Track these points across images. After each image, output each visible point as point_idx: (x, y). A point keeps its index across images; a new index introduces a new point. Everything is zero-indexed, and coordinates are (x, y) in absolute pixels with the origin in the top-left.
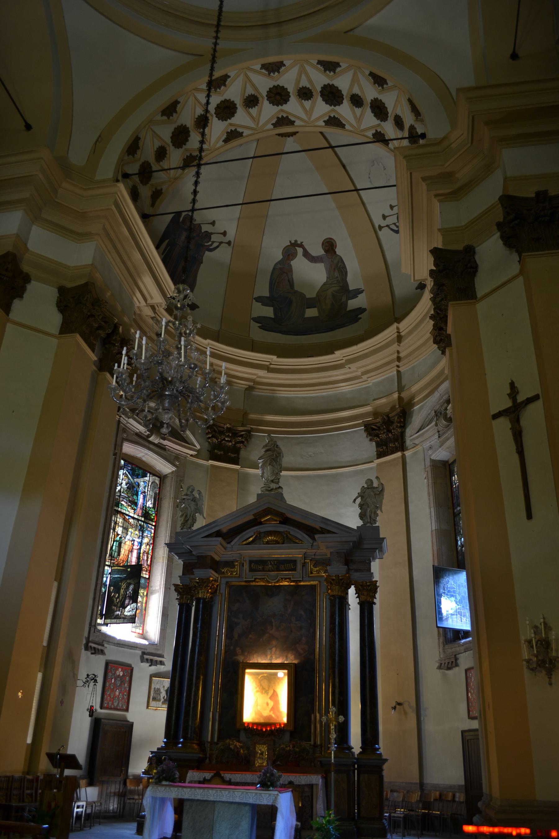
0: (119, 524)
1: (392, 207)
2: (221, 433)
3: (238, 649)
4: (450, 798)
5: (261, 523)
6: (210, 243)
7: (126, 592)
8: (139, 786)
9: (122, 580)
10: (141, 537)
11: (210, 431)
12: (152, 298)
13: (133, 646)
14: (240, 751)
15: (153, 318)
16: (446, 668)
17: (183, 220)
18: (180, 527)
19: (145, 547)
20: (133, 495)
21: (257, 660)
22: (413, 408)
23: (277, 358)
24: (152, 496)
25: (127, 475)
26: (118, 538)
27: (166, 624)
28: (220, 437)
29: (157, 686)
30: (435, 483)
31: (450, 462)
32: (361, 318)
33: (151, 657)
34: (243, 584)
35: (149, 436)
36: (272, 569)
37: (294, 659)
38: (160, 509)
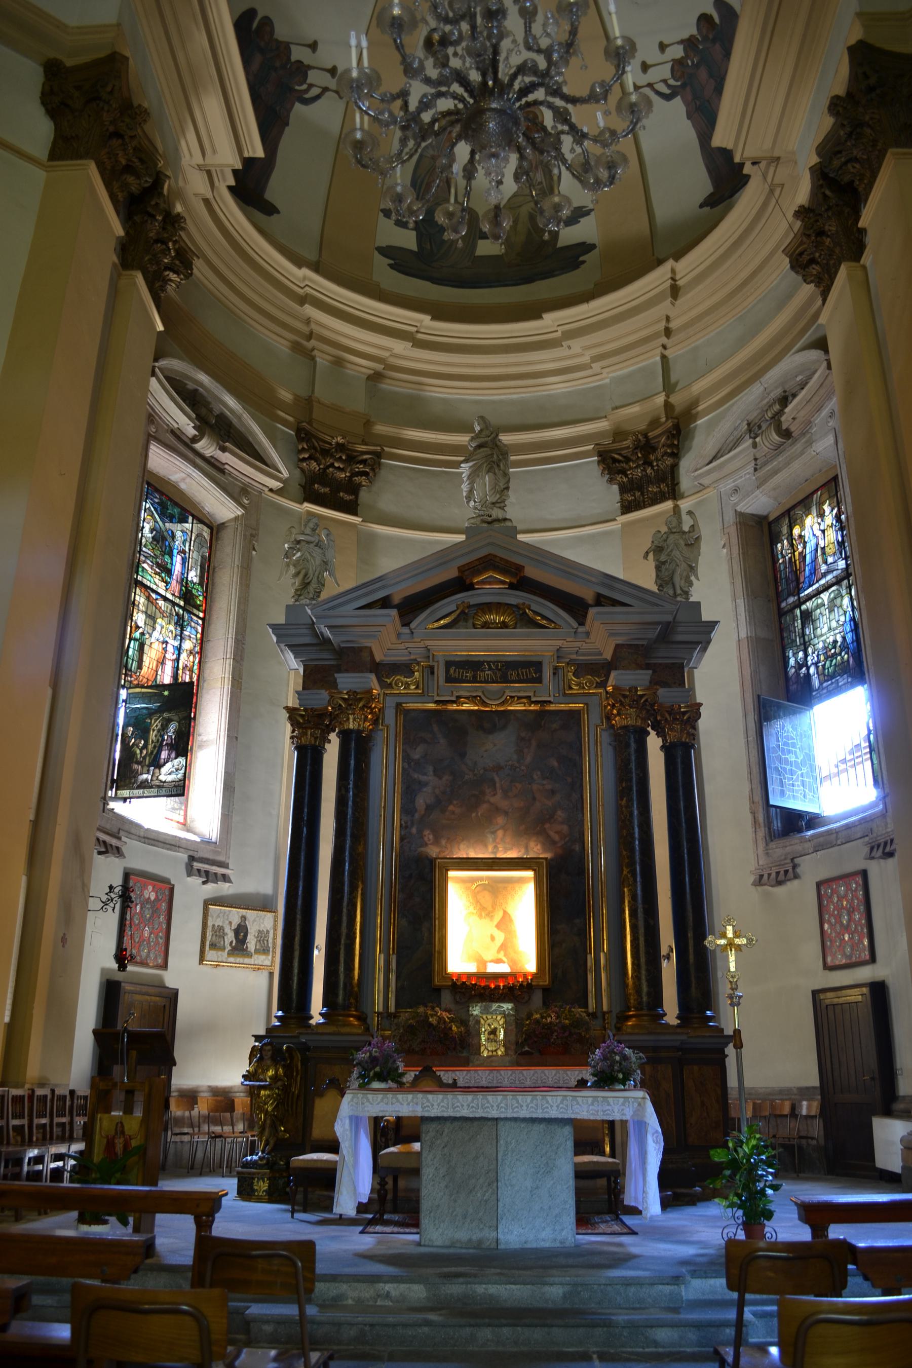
0: (138, 606)
1: (662, 47)
2: (326, 453)
3: (426, 832)
4: (787, 1110)
5: (471, 587)
6: (304, 87)
7: (162, 736)
8: (193, 1109)
9: (151, 713)
10: (179, 638)
11: (305, 446)
12: (214, 151)
13: (173, 843)
14: (451, 1028)
15: (206, 201)
16: (774, 882)
17: (258, 26)
19: (186, 658)
21: (467, 854)
22: (695, 421)
23: (431, 320)
26: (137, 635)
27: (231, 804)
28: (323, 461)
29: (219, 923)
30: (744, 554)
31: (771, 518)
32: (583, 262)
34: (432, 706)
35: (195, 440)
37: (541, 851)
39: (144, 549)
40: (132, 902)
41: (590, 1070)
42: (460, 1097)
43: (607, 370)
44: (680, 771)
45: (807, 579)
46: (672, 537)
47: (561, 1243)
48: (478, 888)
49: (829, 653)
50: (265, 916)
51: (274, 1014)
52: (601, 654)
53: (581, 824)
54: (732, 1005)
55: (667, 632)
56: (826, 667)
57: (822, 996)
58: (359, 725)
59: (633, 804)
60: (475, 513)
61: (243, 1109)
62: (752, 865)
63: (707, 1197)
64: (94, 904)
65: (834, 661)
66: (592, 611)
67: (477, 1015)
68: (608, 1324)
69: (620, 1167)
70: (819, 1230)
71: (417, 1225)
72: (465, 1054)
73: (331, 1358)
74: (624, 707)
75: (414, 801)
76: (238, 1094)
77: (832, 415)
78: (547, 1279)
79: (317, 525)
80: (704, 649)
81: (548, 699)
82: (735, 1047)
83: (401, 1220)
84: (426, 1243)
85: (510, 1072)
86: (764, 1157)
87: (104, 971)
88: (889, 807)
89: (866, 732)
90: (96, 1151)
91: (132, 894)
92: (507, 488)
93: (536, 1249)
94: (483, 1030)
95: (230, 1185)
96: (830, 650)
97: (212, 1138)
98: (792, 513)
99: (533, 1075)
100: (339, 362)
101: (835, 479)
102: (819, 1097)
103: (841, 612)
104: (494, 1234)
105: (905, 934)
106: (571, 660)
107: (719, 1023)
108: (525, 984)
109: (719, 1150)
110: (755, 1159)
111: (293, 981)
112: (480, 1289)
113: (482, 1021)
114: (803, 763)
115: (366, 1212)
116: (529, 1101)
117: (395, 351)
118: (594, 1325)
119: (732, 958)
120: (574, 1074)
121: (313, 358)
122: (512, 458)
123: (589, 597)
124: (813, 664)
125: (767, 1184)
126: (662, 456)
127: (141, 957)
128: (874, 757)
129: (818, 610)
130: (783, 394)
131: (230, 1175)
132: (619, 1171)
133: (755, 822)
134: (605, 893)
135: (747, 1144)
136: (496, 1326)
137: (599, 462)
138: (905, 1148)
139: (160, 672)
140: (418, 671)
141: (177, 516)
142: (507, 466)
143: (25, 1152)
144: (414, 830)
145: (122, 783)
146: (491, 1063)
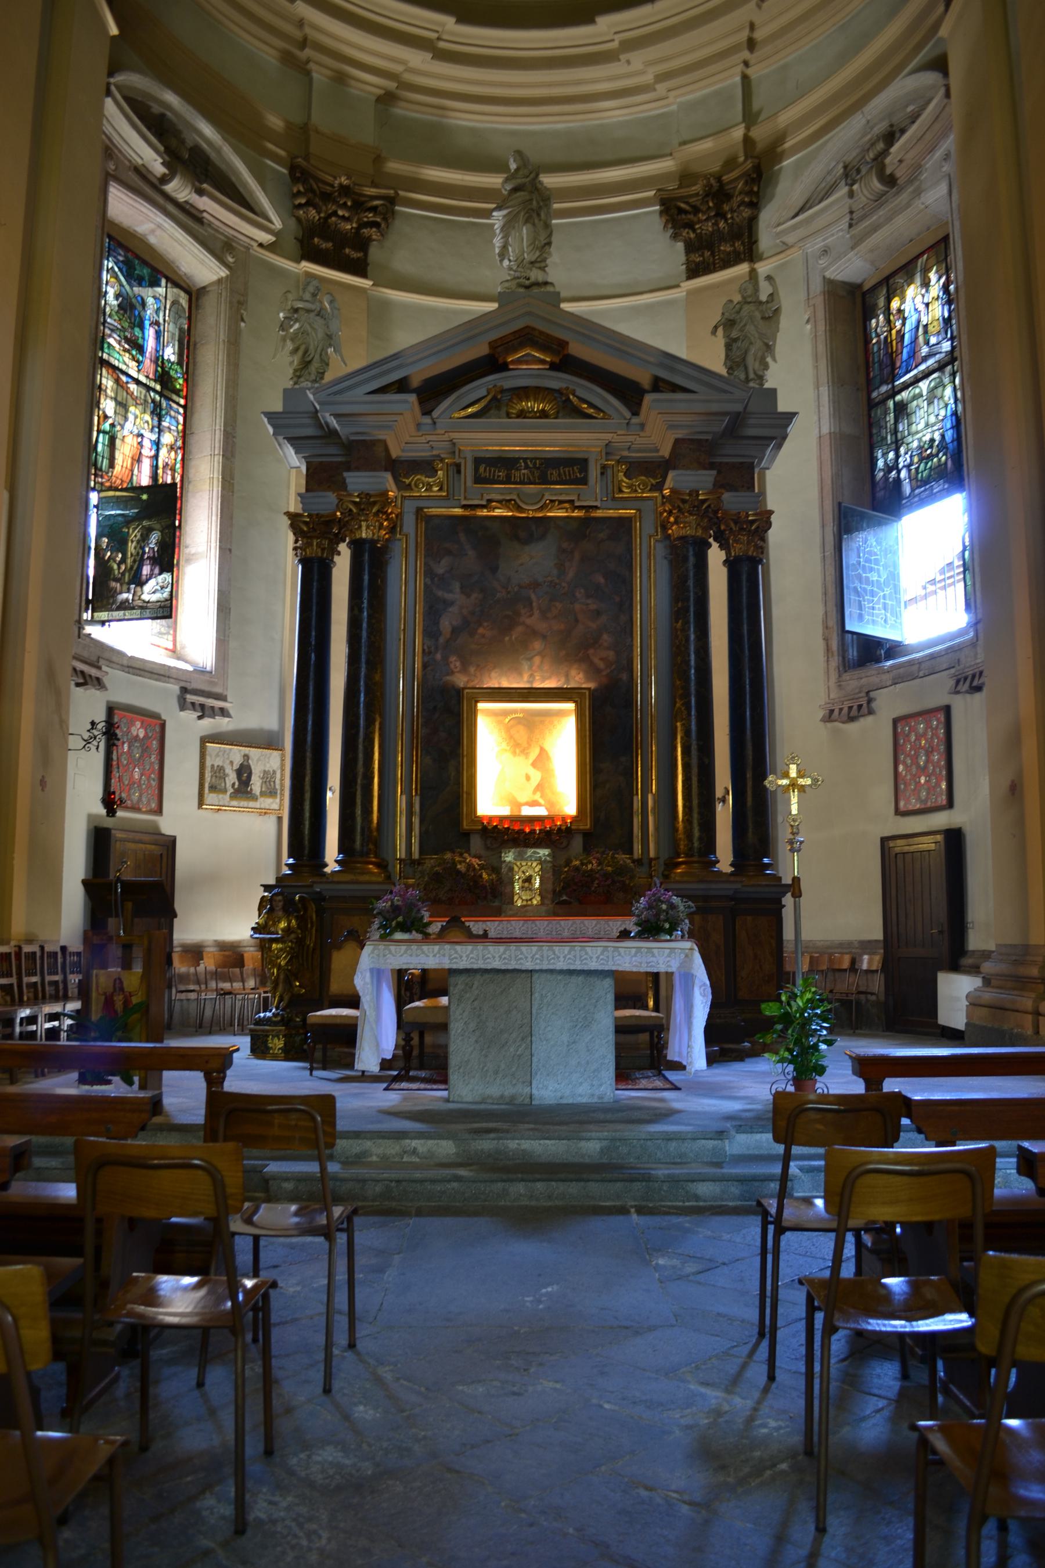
0: (105, 391)
2: (327, 197)
3: (453, 659)
4: (846, 964)
5: (504, 367)
7: (143, 548)
8: (199, 965)
9: (128, 521)
10: (157, 430)
11: (302, 189)
14: (481, 876)
18: (292, 379)
19: (167, 455)
20: (132, 326)
21: (499, 683)
24: (173, 334)
25: (116, 273)
26: (106, 426)
28: (324, 208)
29: (218, 762)
30: (832, 331)
31: (866, 287)
33: (201, 700)
34: (458, 511)
35: (164, 180)
36: (529, 478)
38: (194, 369)
39: (109, 320)
40: (118, 740)
41: (634, 919)
42: (491, 948)
43: (673, 94)
44: (744, 590)
45: (904, 364)
46: (746, 308)
47: (599, 1098)
48: (512, 722)
49: (925, 454)
50: (271, 754)
51: (284, 862)
52: (657, 451)
53: (630, 648)
54: (792, 850)
55: (736, 422)
56: (920, 470)
57: (891, 844)
58: (374, 534)
59: (689, 628)
60: (509, 274)
61: (254, 964)
62: (822, 698)
63: (755, 1053)
64: (74, 742)
65: (930, 464)
66: (648, 398)
67: (510, 862)
68: (647, 1178)
69: (664, 1021)
70: (873, 1082)
71: (445, 1080)
72: (497, 904)
73: (355, 1212)
74: (683, 514)
75: (438, 623)
76: (247, 949)
77: (947, 157)
78: (584, 1134)
79: (318, 289)
80: (779, 446)
81: (595, 504)
82: (793, 896)
83: (427, 1076)
84: (456, 1100)
85: (546, 923)
86: (819, 1011)
87: (91, 817)
88: (981, 636)
89: (961, 549)
90: (94, 1008)
91: (118, 731)
92: (549, 244)
93: (573, 1104)
94: (517, 877)
95: (244, 1042)
96: (926, 450)
97: (222, 995)
98: (891, 281)
99: (572, 926)
100: (340, 79)
101: (946, 239)
102: (882, 951)
103: (942, 405)
104: (527, 1090)
105: (987, 777)
106: (622, 457)
107: (777, 871)
108: (564, 828)
109: (771, 1004)
110: (809, 1013)
111: (304, 825)
112: (512, 1145)
113: (516, 869)
114: (887, 583)
115: (390, 1069)
116: (566, 952)
117: (411, 64)
118: (632, 1180)
119: (794, 800)
120: (616, 924)
121: (308, 73)
122: (556, 206)
123: (645, 382)
124: (904, 466)
125: (821, 1039)
126: (739, 206)
127: (132, 801)
128: (968, 577)
129: (915, 403)
130: (889, 129)
131: (242, 1033)
132: (662, 1025)
133: (828, 650)
134: (655, 728)
135: (801, 997)
136: (530, 1181)
137: (661, 213)
138: (971, 1004)
139: (136, 472)
140: (441, 470)
141: (147, 278)
142: (550, 215)
143: (15, 1012)
144: (438, 656)
145: (99, 604)
146: (525, 912)
